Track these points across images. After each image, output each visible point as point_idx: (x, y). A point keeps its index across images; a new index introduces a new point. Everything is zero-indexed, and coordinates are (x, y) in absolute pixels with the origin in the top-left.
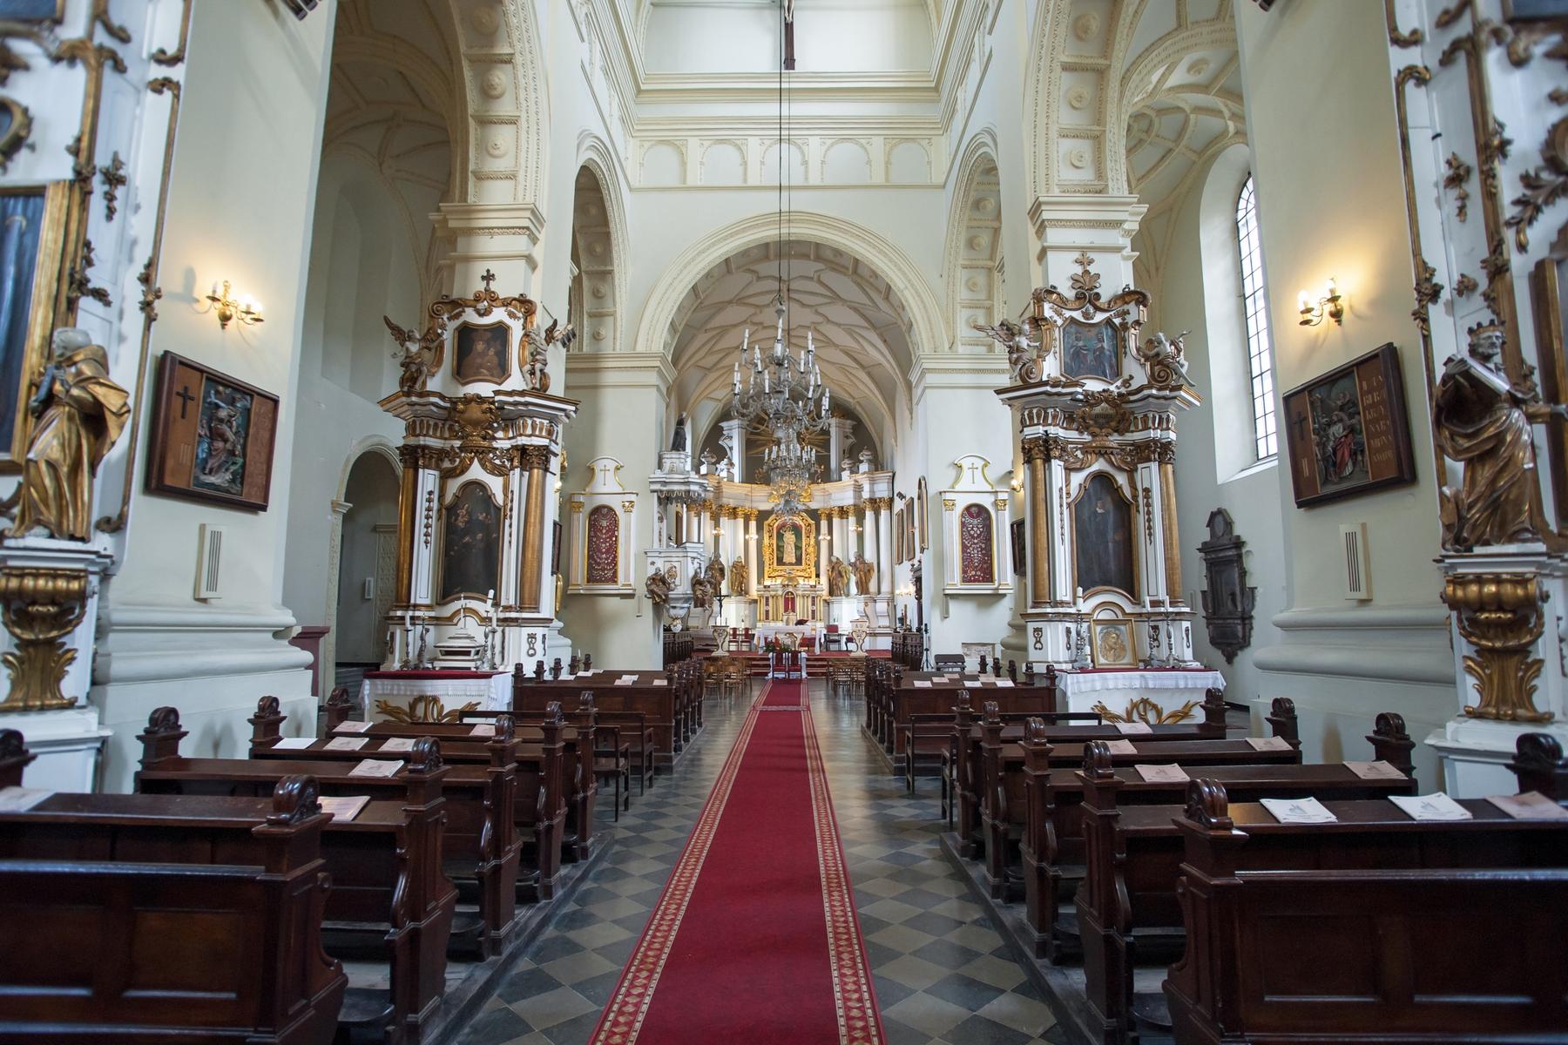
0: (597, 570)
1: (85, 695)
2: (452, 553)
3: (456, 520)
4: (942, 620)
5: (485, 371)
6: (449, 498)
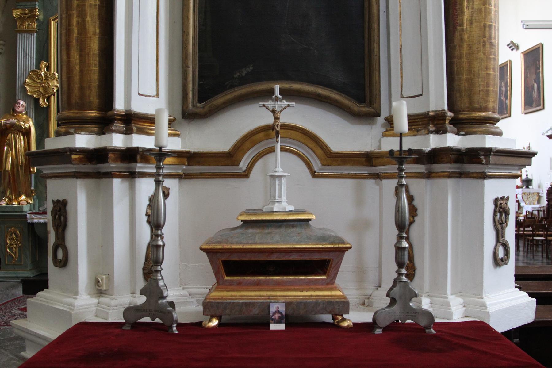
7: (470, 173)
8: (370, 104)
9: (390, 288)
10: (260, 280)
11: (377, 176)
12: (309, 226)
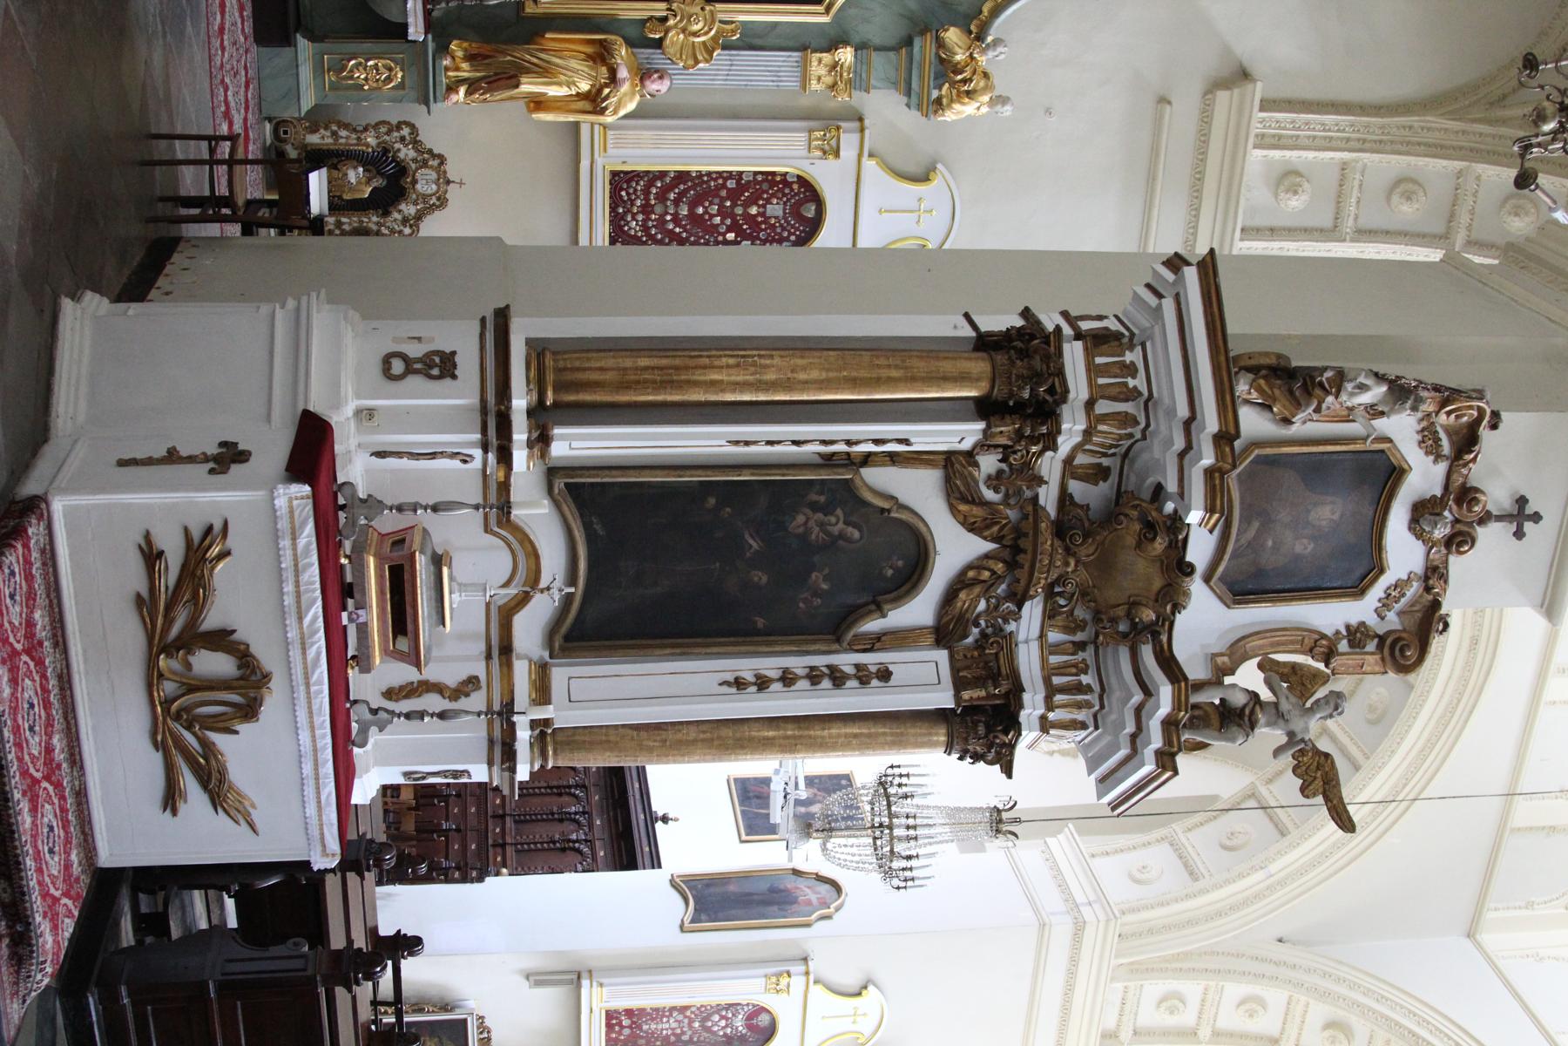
0: (646, 192)
1: (273, 705)
2: (712, 501)
3: (815, 507)
4: (521, 972)
5: (1251, 534)
6: (878, 478)
7: (493, 750)
8: (563, 649)
9: (393, 711)
10: (386, 594)
11: (489, 657)
12: (438, 625)
